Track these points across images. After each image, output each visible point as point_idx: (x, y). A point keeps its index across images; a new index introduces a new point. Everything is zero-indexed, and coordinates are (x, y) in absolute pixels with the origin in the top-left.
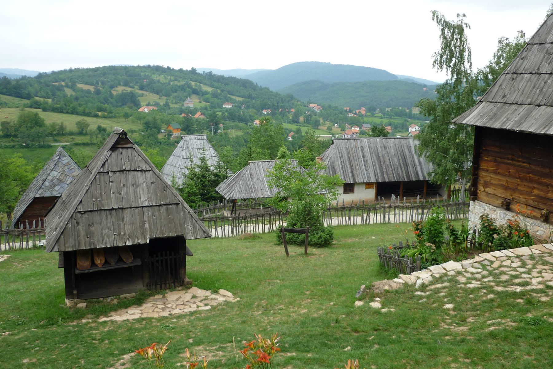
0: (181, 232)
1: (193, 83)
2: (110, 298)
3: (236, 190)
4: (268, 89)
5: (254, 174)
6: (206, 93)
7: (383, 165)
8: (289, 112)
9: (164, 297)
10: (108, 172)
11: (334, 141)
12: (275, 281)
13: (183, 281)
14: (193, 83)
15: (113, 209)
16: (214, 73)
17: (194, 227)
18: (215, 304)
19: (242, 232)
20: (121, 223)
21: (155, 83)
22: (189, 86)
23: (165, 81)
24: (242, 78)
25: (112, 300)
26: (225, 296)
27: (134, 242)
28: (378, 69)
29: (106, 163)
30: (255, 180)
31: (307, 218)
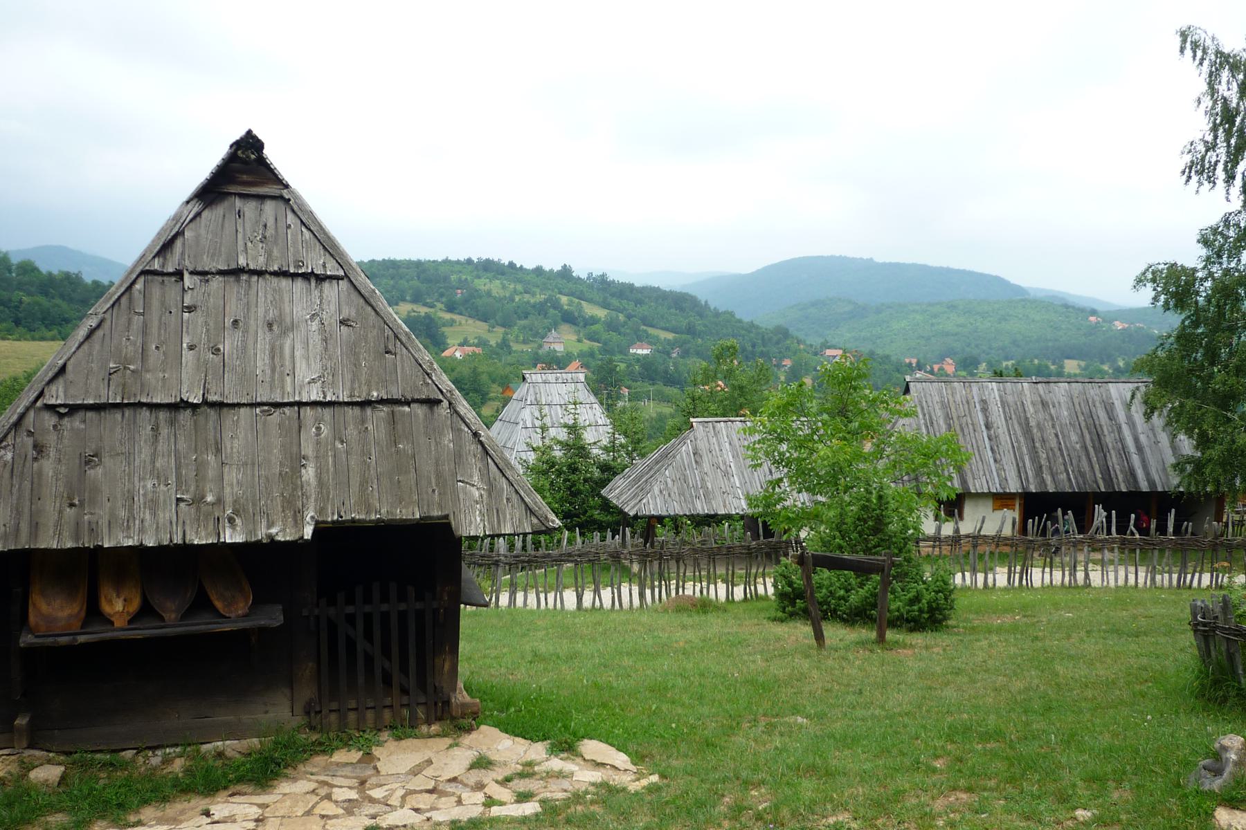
0: (440, 507)
1: (564, 299)
2: (159, 752)
3: (656, 490)
4: (732, 314)
5: (704, 453)
6: (594, 320)
7: (1040, 450)
8: (779, 366)
9: (368, 758)
10: (179, 274)
11: (911, 385)
12: (791, 719)
13: (447, 703)
14: (564, 299)
15: (183, 405)
16: (611, 277)
17: (491, 488)
18: (560, 795)
19: (668, 594)
20: (211, 458)
21: (481, 297)
22: (557, 306)
23: (502, 293)
24: (673, 289)
25: (167, 761)
26: (601, 764)
27: (253, 531)
28: (982, 275)
29: (179, 243)
30: (706, 466)
31: (873, 540)
